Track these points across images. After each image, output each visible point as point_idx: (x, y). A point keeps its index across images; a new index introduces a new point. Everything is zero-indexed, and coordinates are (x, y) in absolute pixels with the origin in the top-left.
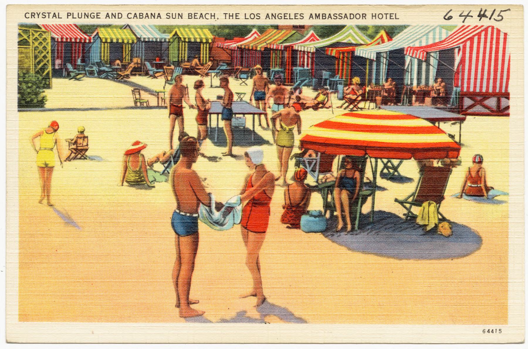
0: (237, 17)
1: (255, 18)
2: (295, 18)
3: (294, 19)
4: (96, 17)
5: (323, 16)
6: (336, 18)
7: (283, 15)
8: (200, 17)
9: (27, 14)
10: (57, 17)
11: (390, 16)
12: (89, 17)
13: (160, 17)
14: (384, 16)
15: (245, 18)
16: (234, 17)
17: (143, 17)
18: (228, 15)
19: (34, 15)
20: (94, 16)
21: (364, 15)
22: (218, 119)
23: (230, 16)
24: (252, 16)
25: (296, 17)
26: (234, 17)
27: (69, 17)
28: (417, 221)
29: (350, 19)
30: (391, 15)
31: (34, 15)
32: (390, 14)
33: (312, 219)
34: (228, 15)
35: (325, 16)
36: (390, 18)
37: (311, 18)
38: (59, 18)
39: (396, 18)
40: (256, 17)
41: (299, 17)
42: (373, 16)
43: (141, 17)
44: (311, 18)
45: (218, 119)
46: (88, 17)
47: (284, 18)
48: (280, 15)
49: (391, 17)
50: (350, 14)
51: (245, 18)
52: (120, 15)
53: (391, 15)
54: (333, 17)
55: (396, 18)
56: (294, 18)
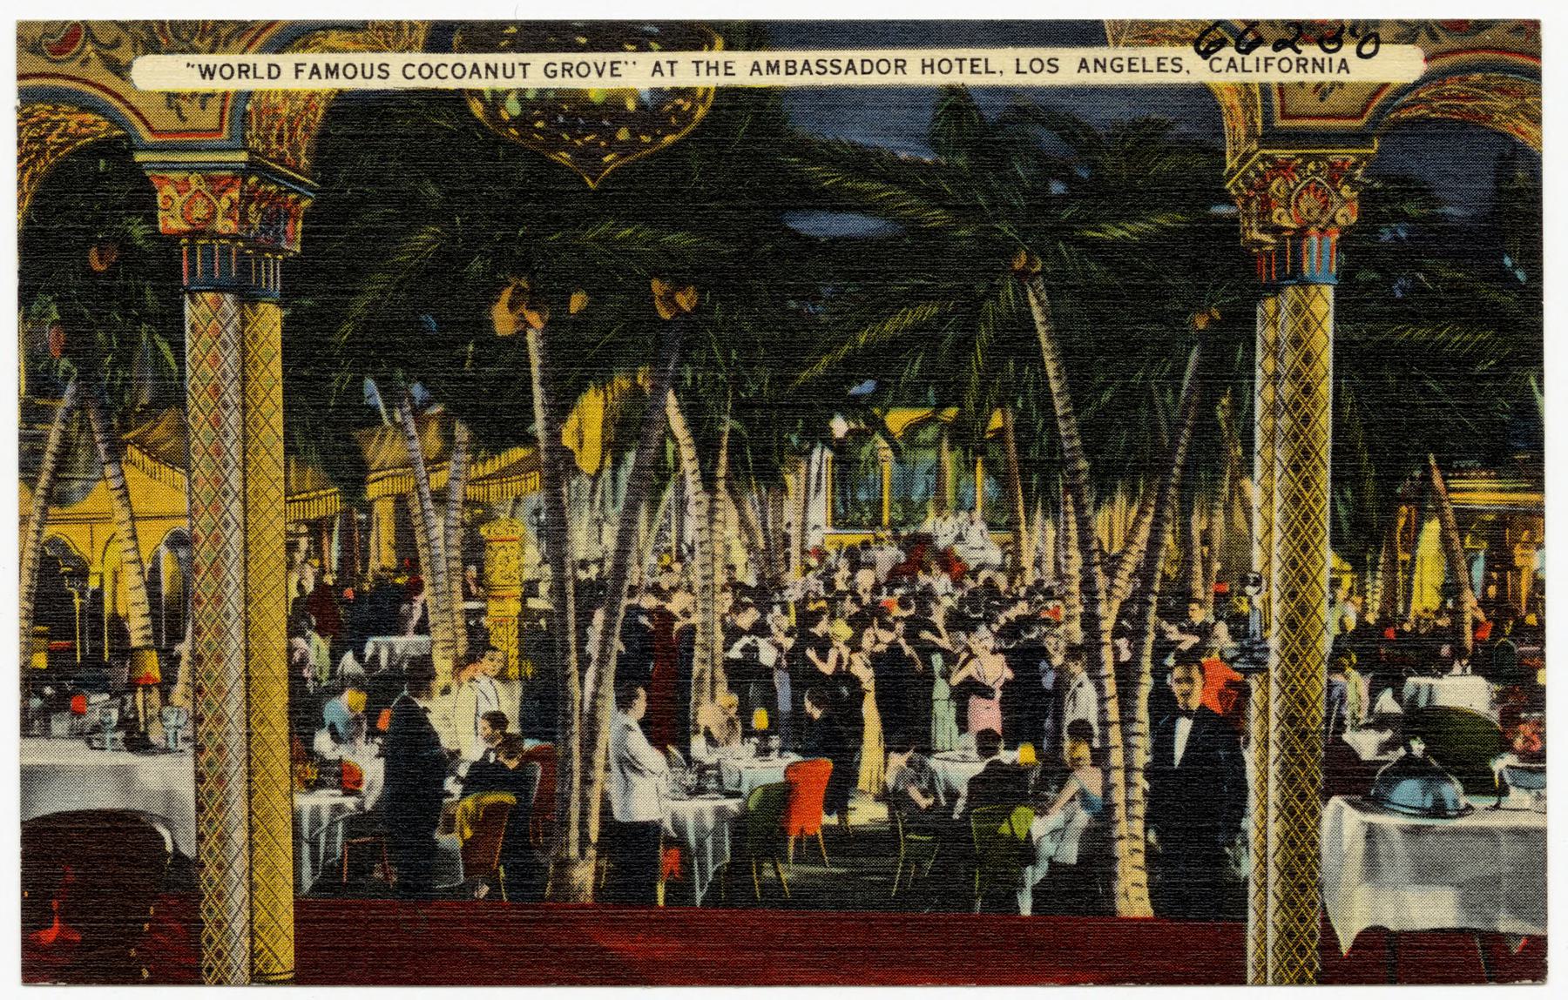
0: (729, 71)
1: (1044, 72)
2: (1159, 71)
3: (1155, 73)
4: (1126, 68)
5: (787, 67)
6: (822, 70)
7: (1125, 63)
8: (1229, 66)
9: (408, 69)
10: (1239, 67)
11: (973, 66)
12: (574, 72)
13: (1346, 67)
14: (956, 65)
15: (1018, 72)
16: (721, 69)
17: (796, 71)
18: (703, 67)
19: (246, 72)
20: (1121, 66)
21: (900, 63)
22: (174, 516)
23: (709, 68)
24: (1037, 66)
25: (1162, 68)
26: (721, 69)
27: (1269, 68)
28: (446, 789)
29: (863, 73)
30: (975, 63)
31: (246, 72)
32: (972, 60)
33: (1366, 704)
34: (703, 67)
35: (794, 67)
36: (972, 72)
37: (315, 77)
38: (1244, 71)
39: (987, 72)
40: (1047, 67)
41: (1169, 66)
42: (924, 66)
43: (791, 70)
44: (315, 77)
45: (174, 516)
46: (1104, 68)
47: (1130, 70)
48: (1116, 62)
49: (975, 69)
50: (863, 61)
51: (1018, 72)
52: (274, 70)
53: (975, 63)
54: (814, 68)
55: (987, 72)
56: (1155, 69)
